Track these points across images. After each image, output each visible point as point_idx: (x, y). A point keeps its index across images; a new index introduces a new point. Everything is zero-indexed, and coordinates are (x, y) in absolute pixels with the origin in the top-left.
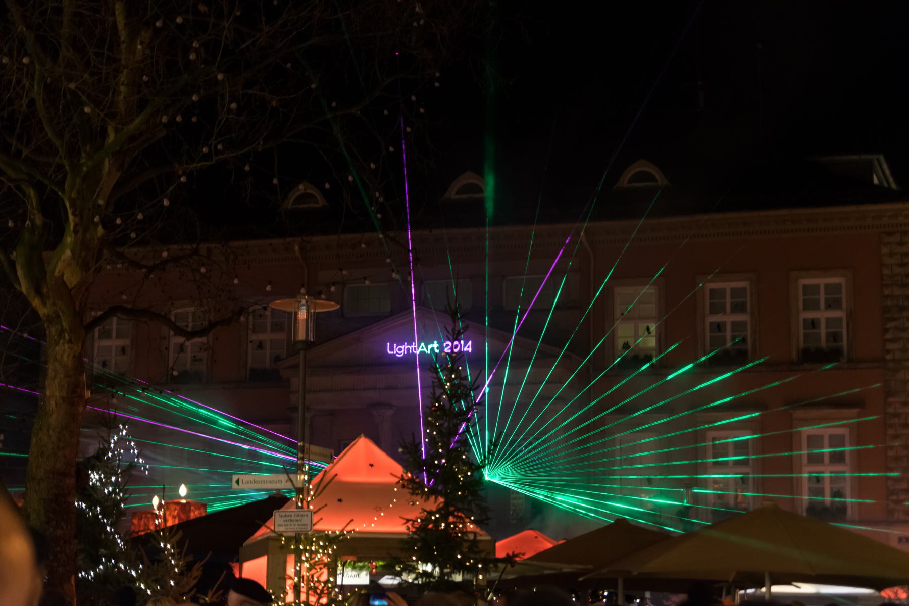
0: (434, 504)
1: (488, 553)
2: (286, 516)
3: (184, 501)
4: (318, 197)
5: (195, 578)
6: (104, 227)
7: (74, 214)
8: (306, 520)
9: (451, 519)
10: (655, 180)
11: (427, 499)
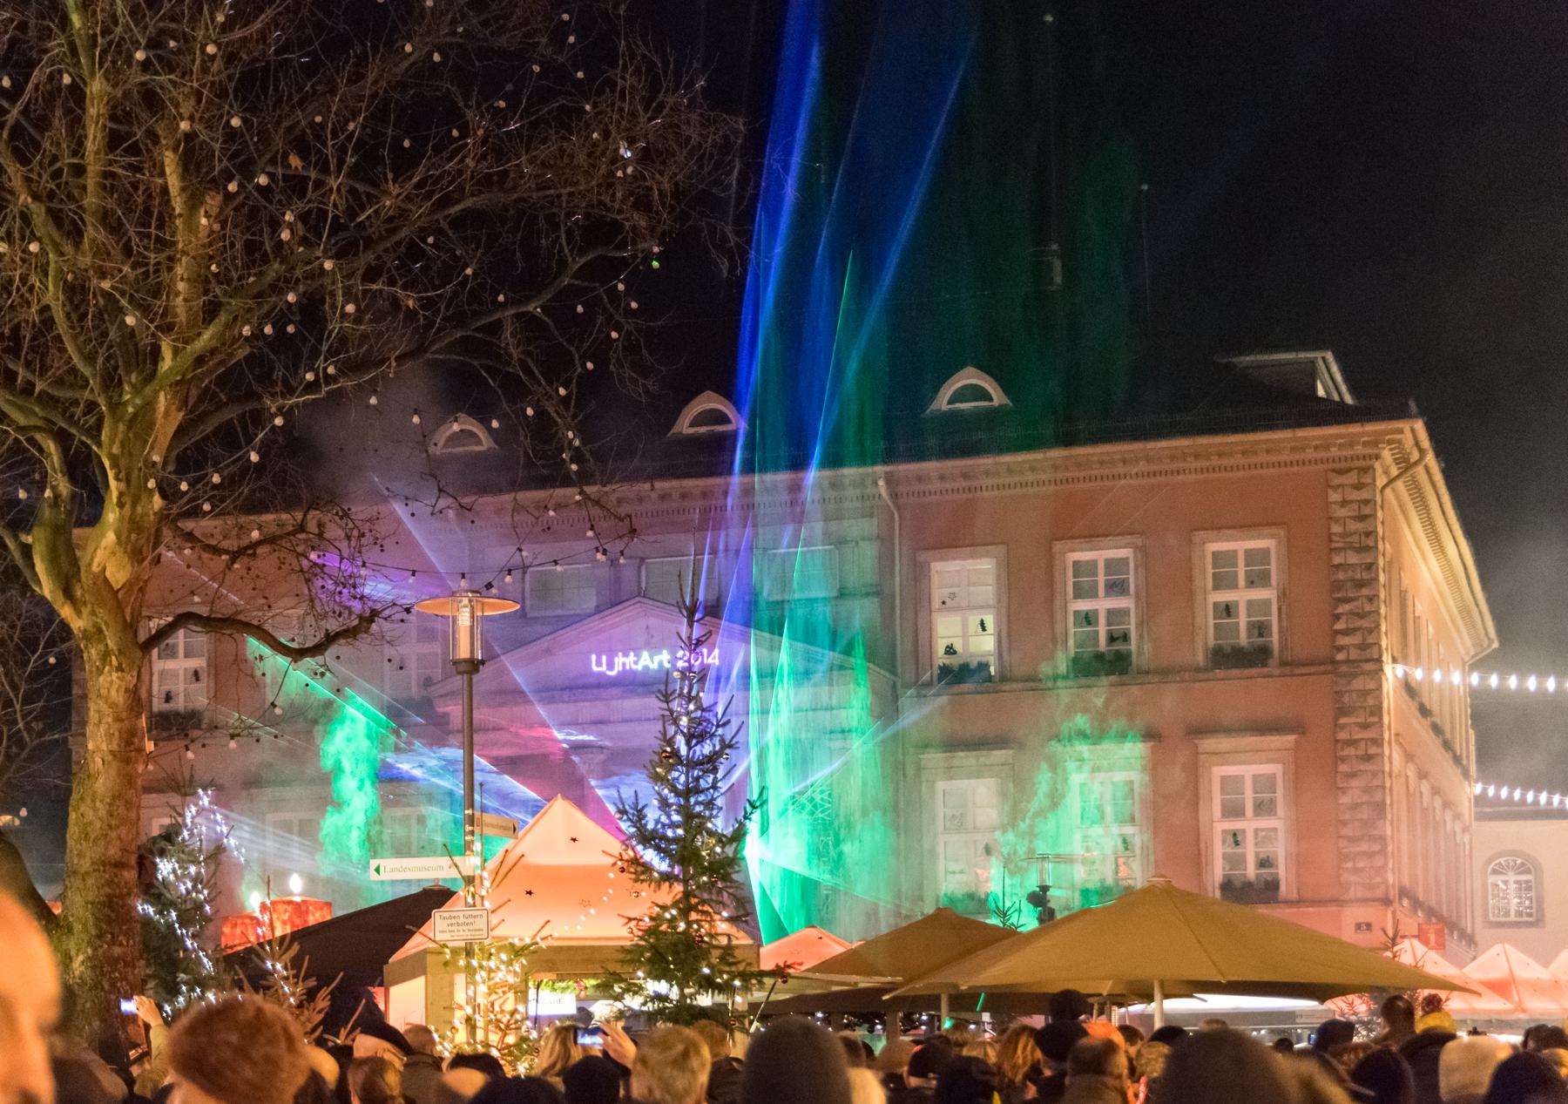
6: (163, 495)
7: (117, 479)
10: (991, 399)
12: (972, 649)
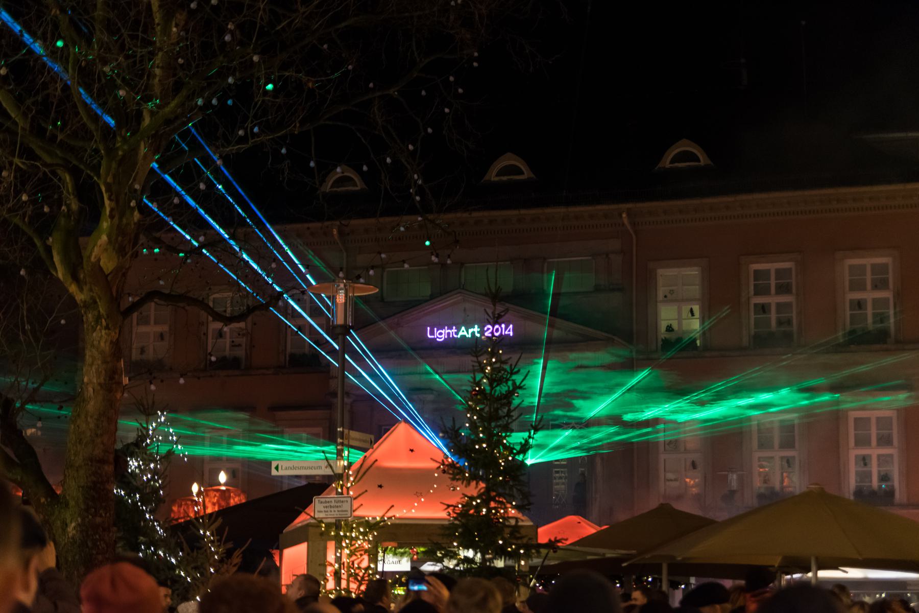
0: (475, 489)
2: (326, 502)
3: (223, 488)
4: (356, 179)
5: (235, 566)
7: (110, 199)
8: (346, 507)
9: (493, 504)
10: (699, 161)
11: (468, 484)
12: (685, 328)
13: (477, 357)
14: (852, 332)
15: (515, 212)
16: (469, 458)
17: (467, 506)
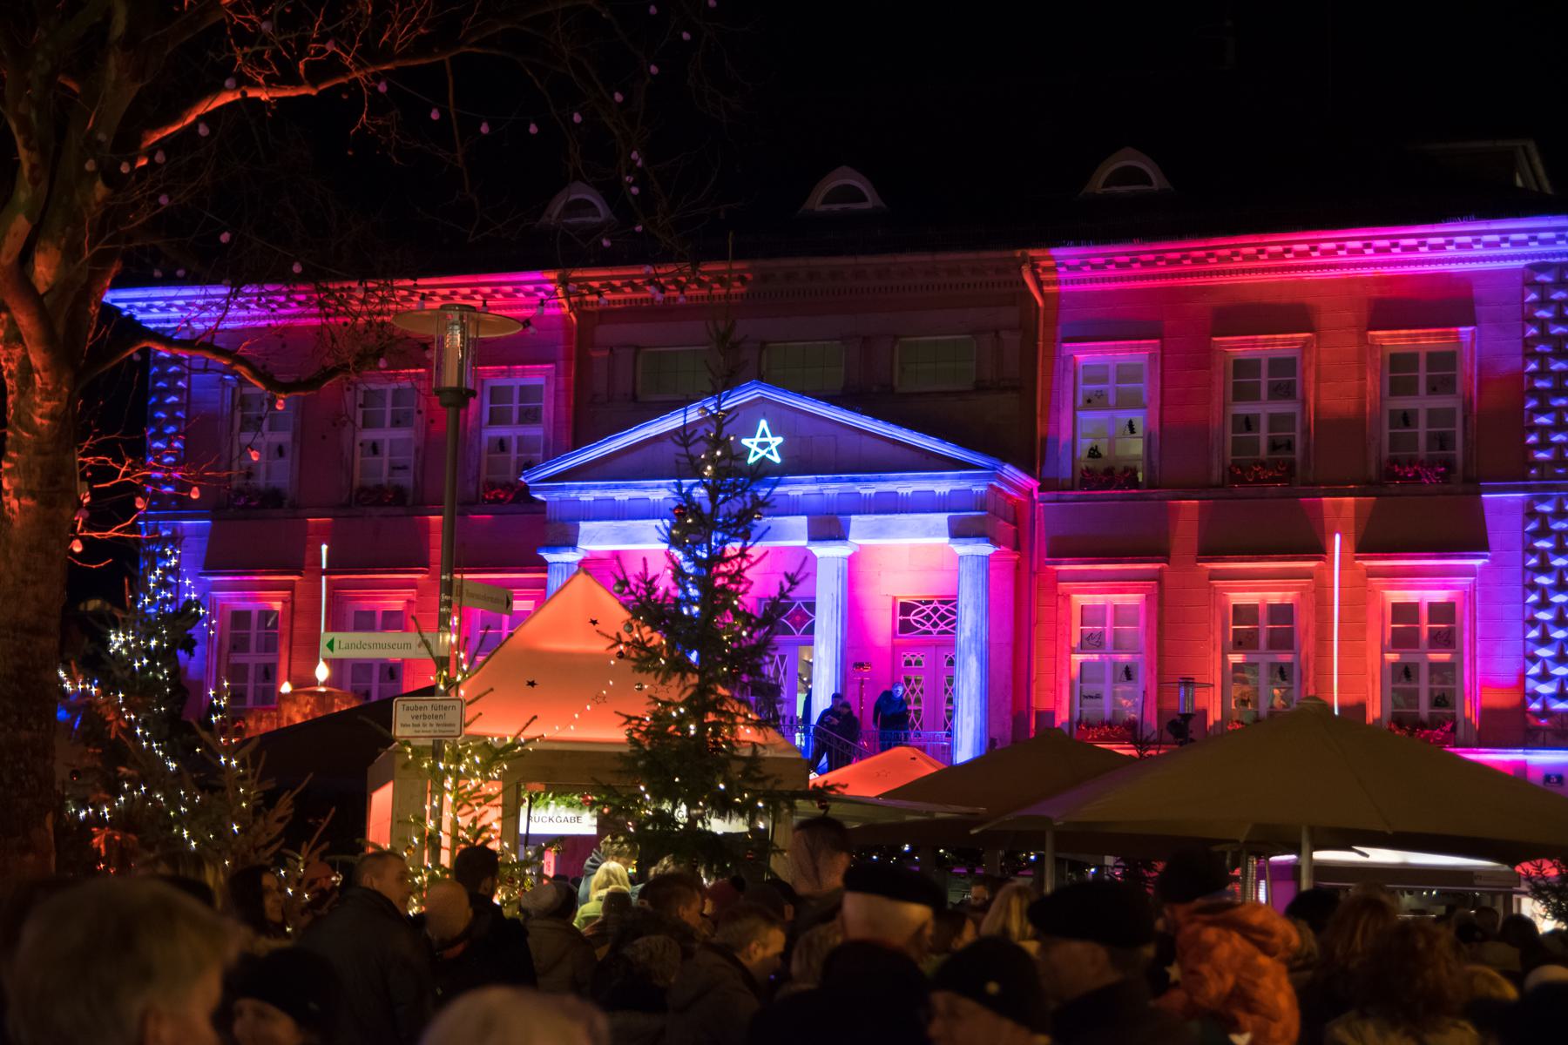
0: (676, 691)
1: (778, 782)
2: (416, 708)
3: (323, 689)
4: (599, 206)
5: (280, 820)
6: (107, 183)
7: (27, 145)
8: (452, 717)
9: (711, 717)
10: (1150, 183)
11: (667, 678)
12: (1119, 452)
13: (686, 446)
14: (1394, 461)
15: (849, 261)
16: (668, 631)
17: (660, 718)
